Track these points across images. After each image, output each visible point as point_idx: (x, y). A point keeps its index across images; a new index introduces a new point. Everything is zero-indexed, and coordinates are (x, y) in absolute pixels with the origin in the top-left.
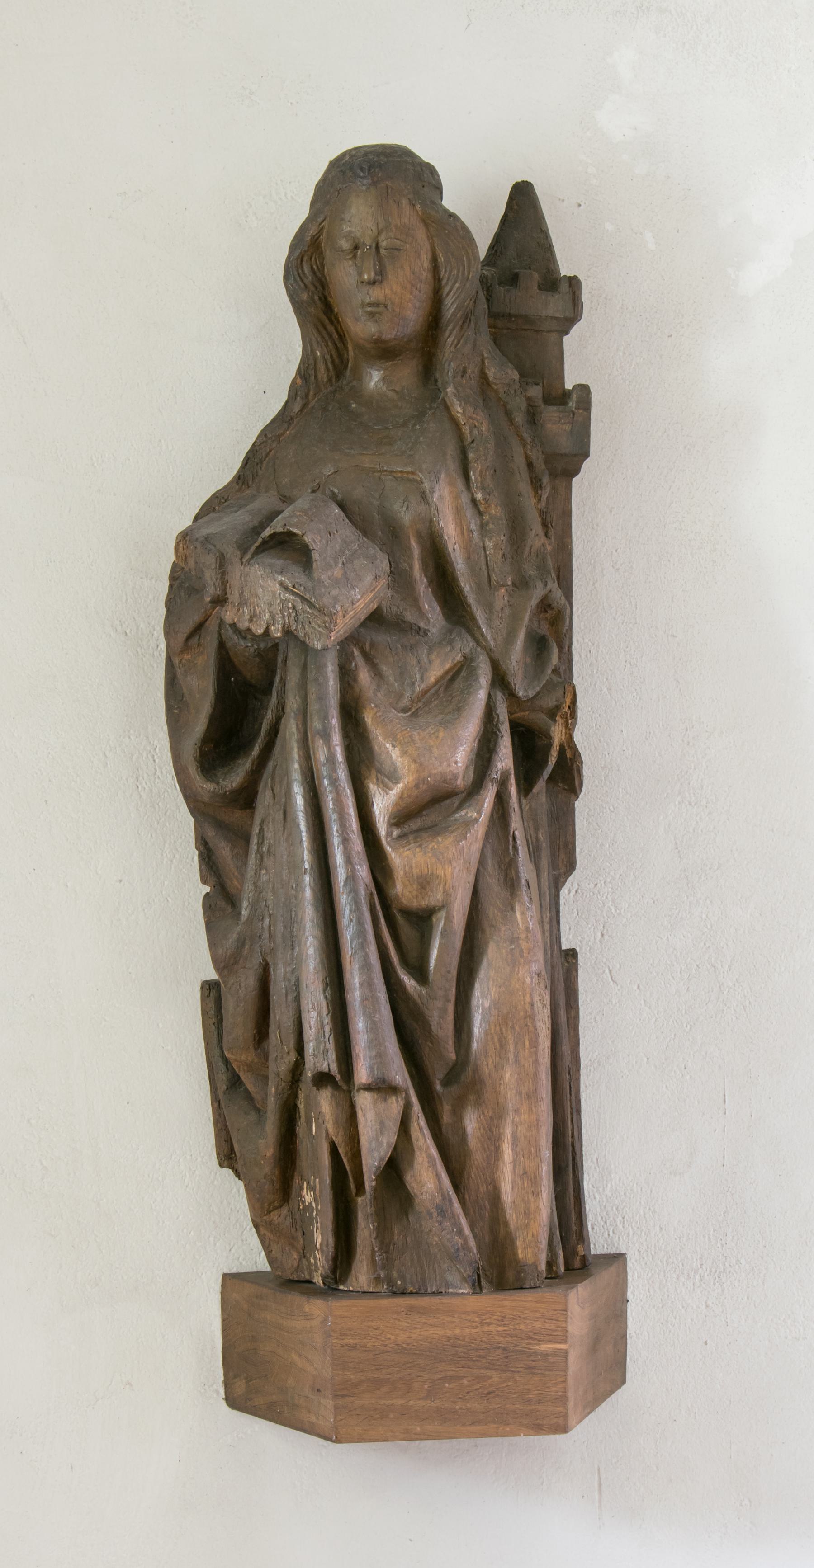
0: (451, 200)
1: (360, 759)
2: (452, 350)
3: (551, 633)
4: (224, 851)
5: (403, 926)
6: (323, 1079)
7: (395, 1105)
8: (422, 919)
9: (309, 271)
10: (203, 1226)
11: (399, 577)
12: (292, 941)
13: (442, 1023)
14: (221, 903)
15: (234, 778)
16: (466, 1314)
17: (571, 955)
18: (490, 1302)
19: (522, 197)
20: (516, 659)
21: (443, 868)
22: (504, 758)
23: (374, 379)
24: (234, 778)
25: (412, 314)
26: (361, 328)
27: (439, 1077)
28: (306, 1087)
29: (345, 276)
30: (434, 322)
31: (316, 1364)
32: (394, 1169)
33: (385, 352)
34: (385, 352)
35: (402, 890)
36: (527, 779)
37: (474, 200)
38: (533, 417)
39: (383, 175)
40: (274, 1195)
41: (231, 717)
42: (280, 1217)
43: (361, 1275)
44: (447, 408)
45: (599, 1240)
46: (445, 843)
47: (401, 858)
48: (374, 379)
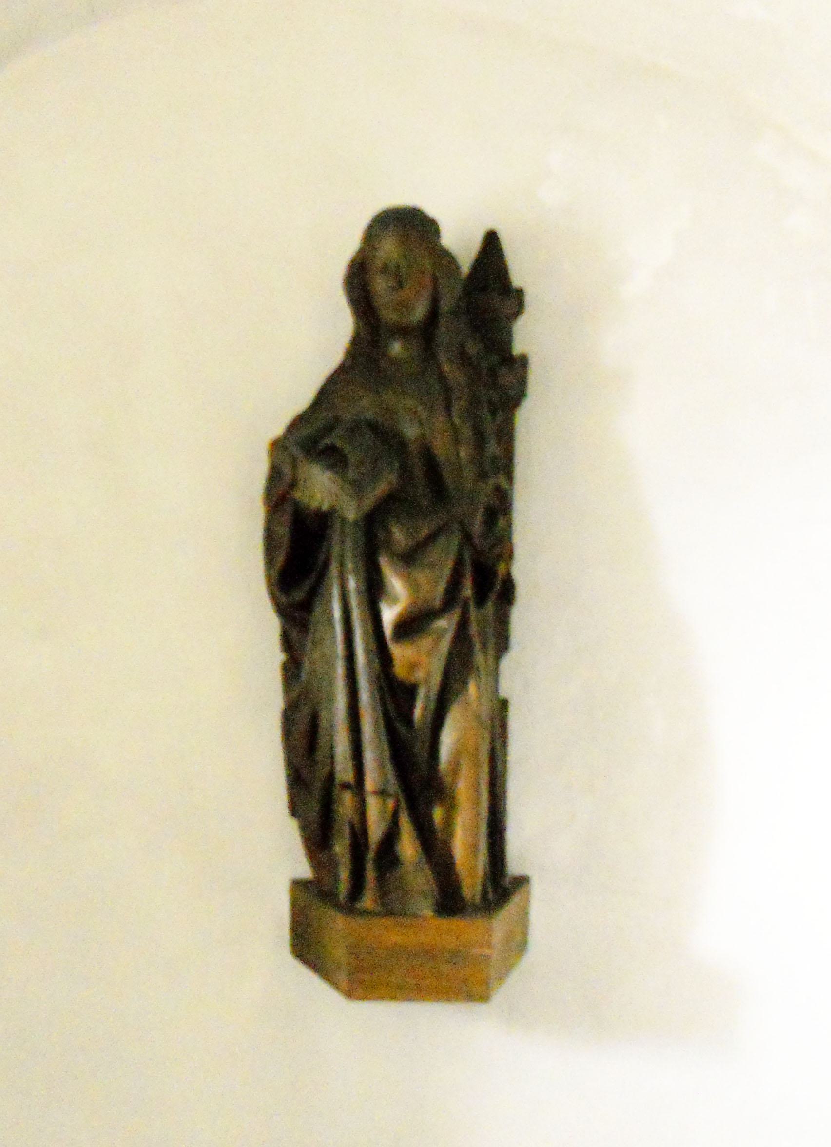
0: (448, 240)
1: (374, 591)
2: (444, 333)
3: (500, 508)
4: (294, 635)
5: (396, 694)
6: (345, 786)
7: (391, 803)
8: (410, 691)
9: (359, 280)
10: (280, 855)
11: (405, 472)
12: (331, 699)
13: (421, 751)
14: (292, 670)
15: (299, 595)
16: (431, 929)
17: (504, 705)
18: (445, 923)
19: (491, 241)
20: (477, 526)
21: (421, 661)
22: (468, 591)
23: (396, 348)
24: (299, 595)
25: (419, 312)
26: (389, 316)
27: (419, 783)
28: (336, 791)
29: (380, 285)
30: (433, 315)
31: (339, 953)
32: (391, 837)
33: (402, 331)
34: (402, 331)
35: (400, 670)
36: (481, 599)
37: (460, 240)
38: (493, 373)
39: (408, 227)
40: (318, 840)
41: (298, 555)
42: (323, 857)
43: (368, 901)
44: (439, 367)
45: (515, 865)
46: (425, 643)
47: (400, 652)
48: (396, 348)
